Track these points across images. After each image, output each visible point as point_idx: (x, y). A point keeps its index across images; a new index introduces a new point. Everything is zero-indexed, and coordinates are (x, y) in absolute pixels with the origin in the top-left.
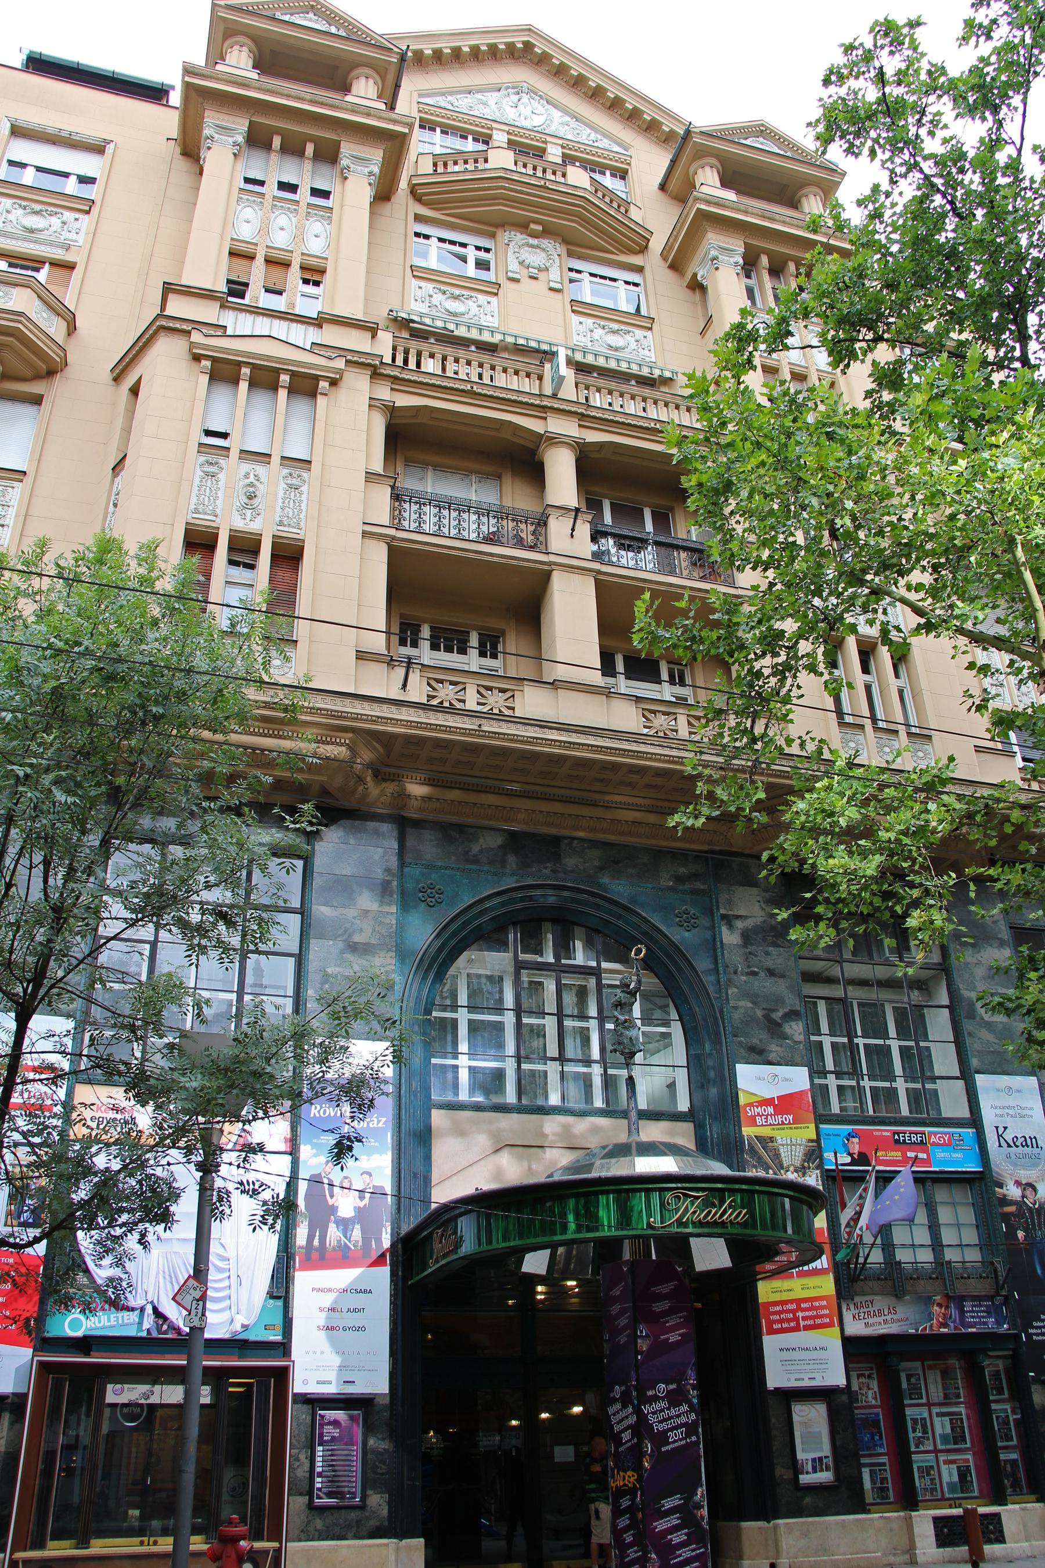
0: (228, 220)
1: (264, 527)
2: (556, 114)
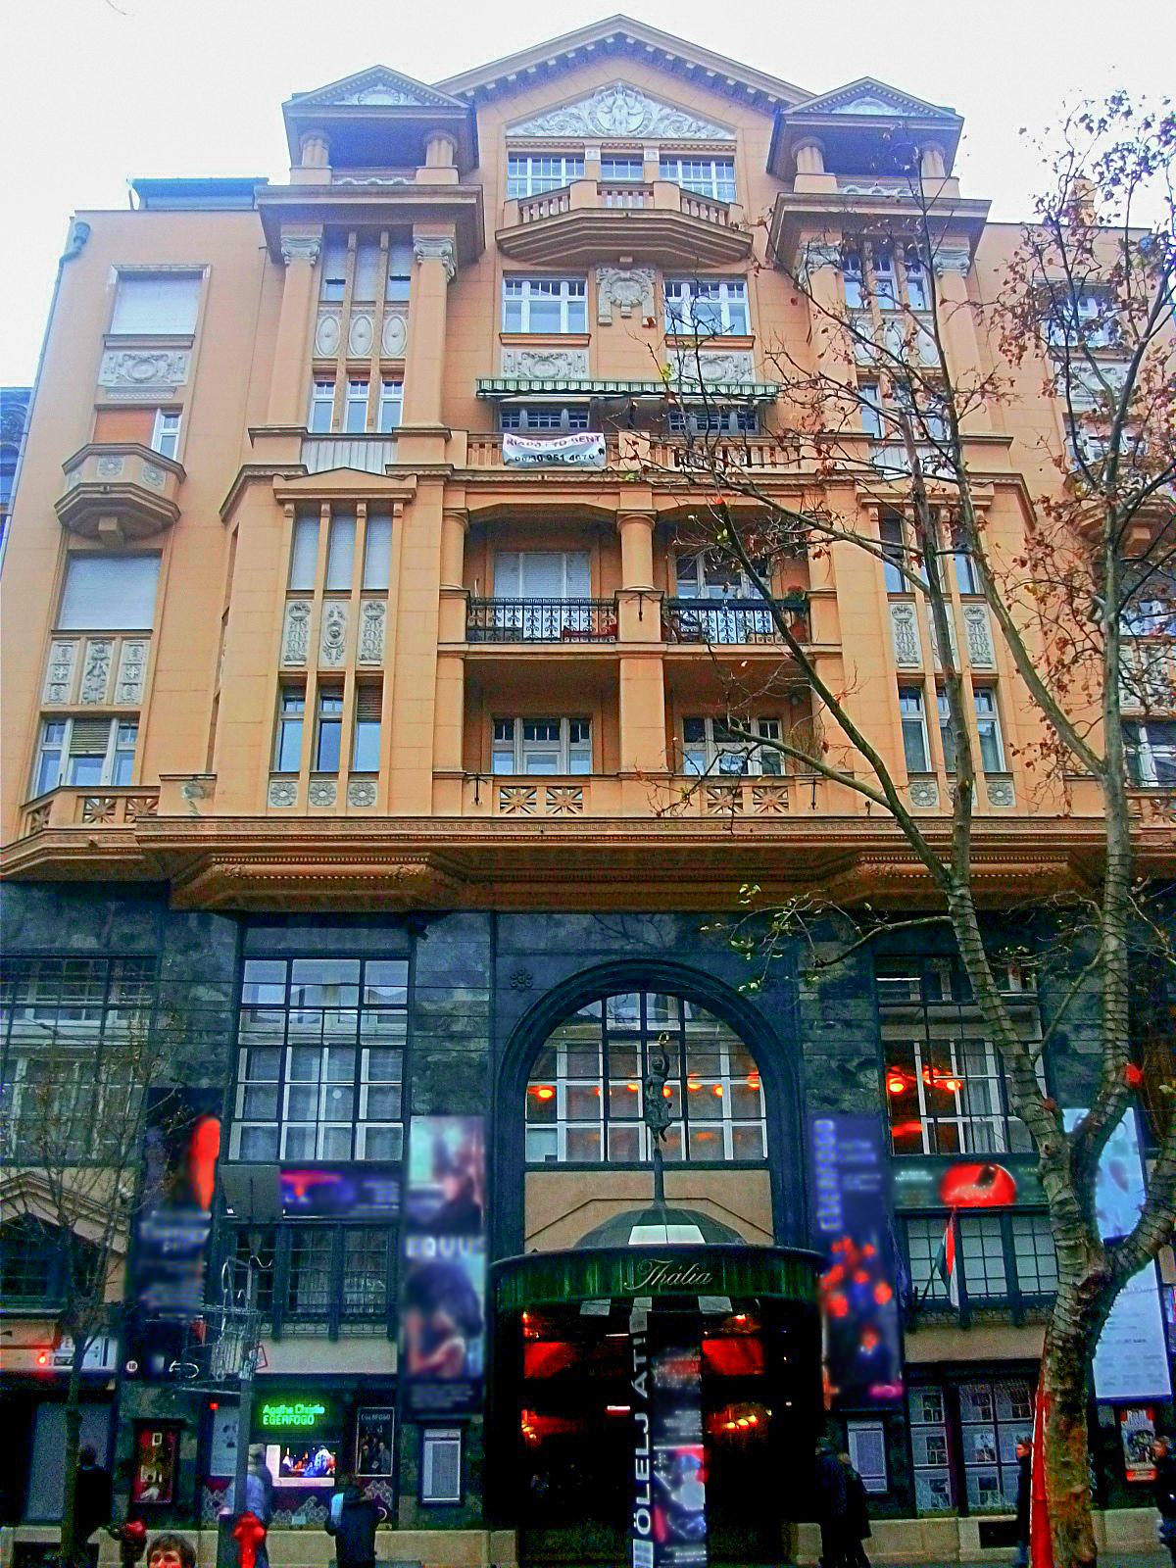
0: (310, 336)
1: (346, 664)
2: (655, 109)
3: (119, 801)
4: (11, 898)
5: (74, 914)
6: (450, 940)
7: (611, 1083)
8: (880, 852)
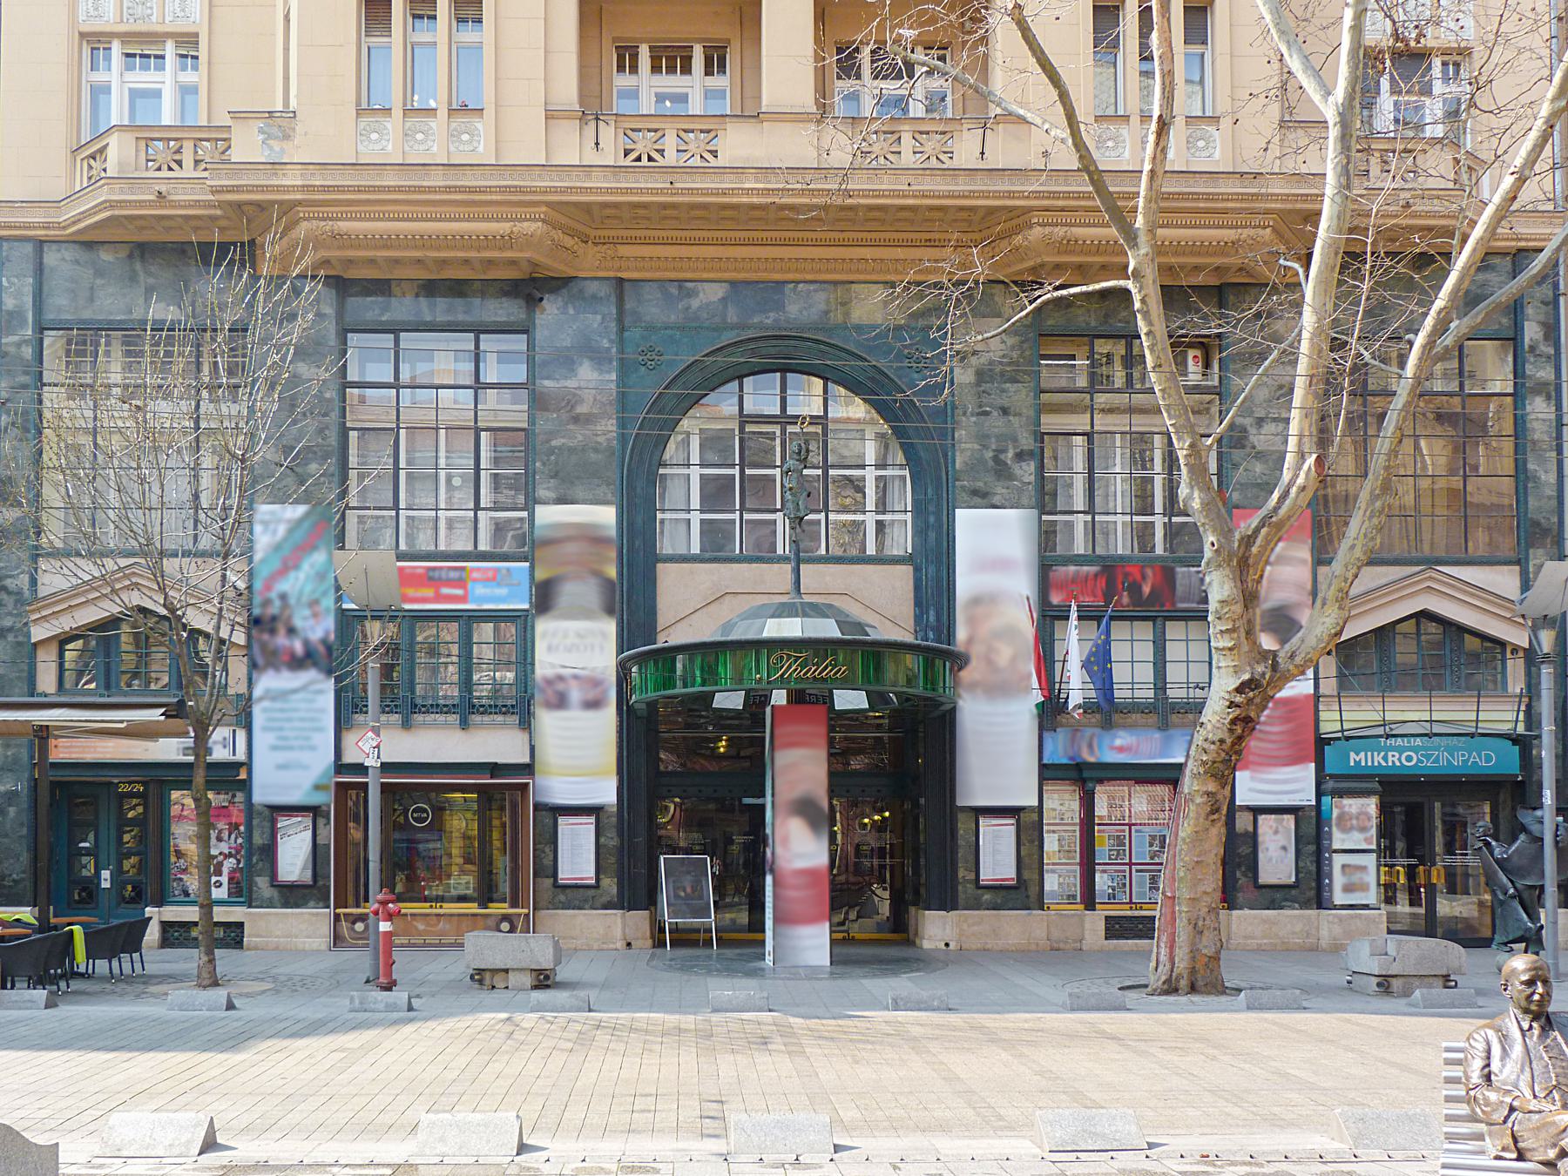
3: (185, 144)
4: (77, 262)
5: (151, 281)
6: (571, 311)
7: (748, 472)
8: (1059, 210)
